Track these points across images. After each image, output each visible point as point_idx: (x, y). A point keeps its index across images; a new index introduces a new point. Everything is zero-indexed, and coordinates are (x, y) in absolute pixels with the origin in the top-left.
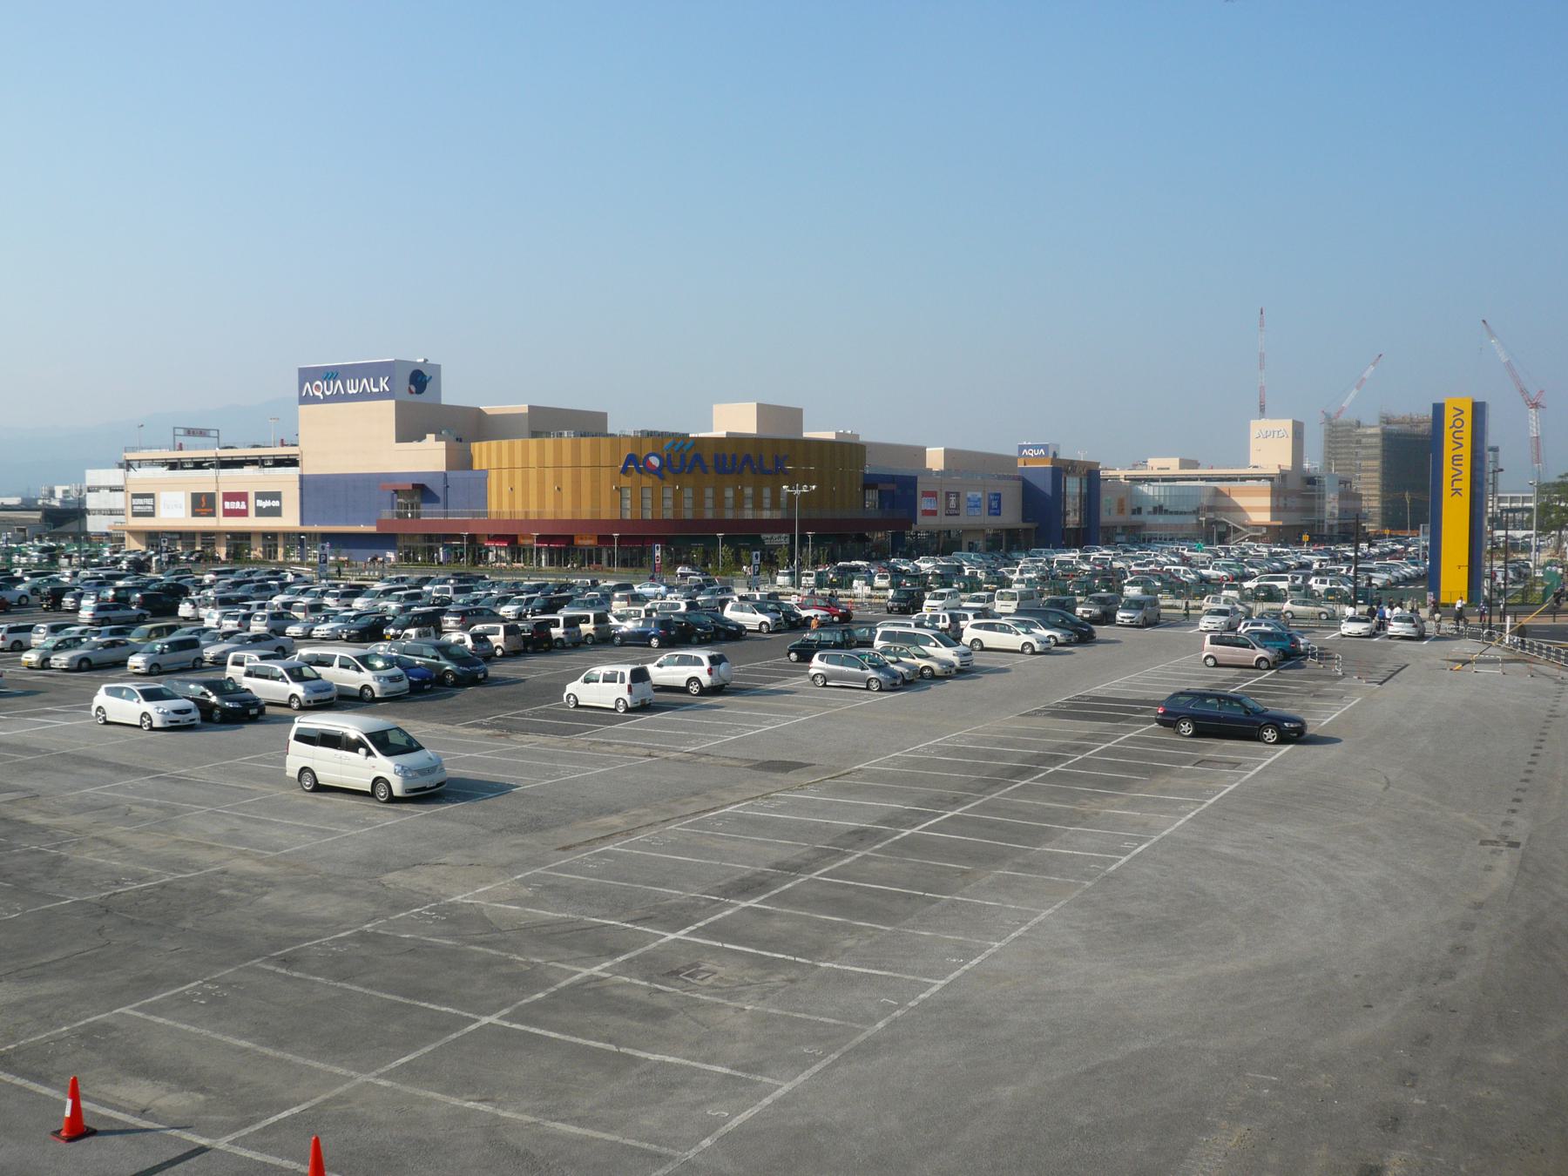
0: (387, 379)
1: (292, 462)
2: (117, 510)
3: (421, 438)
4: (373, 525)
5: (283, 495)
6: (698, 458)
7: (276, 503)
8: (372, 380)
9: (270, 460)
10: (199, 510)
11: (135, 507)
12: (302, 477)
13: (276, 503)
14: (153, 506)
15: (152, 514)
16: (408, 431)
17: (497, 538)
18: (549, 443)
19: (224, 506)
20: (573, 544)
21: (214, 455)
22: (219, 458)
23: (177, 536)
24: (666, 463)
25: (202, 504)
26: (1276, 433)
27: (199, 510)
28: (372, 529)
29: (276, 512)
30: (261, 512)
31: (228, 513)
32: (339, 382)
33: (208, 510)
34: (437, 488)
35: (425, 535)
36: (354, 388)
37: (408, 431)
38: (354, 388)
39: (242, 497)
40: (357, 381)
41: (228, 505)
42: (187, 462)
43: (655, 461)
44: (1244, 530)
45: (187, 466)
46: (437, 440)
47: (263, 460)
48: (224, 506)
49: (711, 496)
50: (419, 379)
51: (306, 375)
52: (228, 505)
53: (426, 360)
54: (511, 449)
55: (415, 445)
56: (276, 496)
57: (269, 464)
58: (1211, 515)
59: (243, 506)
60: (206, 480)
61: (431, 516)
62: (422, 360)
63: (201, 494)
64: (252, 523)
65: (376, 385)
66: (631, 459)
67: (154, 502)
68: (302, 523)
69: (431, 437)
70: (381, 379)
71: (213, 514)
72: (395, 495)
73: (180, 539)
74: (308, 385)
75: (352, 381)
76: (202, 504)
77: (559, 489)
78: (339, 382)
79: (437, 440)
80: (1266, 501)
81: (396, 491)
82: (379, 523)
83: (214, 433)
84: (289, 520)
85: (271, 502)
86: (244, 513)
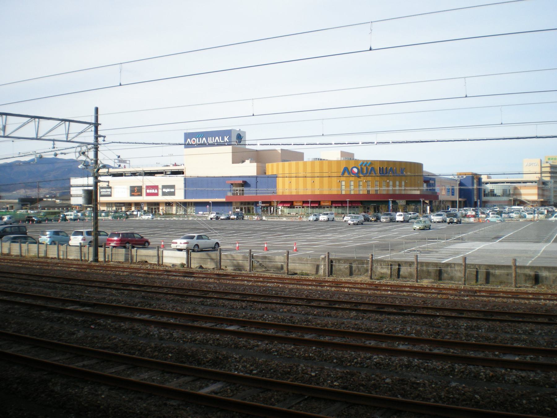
0: (228, 137)
1: (181, 173)
2: (75, 195)
3: (243, 162)
4: (224, 198)
5: (176, 187)
6: (373, 169)
7: (172, 190)
8: (221, 137)
9: (169, 172)
10: (133, 193)
11: (101, 193)
12: (185, 179)
13: (172, 190)
14: (111, 192)
15: (110, 196)
16: (238, 158)
17: (283, 203)
18: (287, 163)
19: (146, 191)
20: (293, 205)
21: (142, 170)
22: (144, 171)
23: (123, 205)
24: (361, 171)
25: (136, 191)
26: (534, 164)
27: (133, 193)
28: (224, 200)
29: (173, 194)
30: (164, 194)
31: (148, 194)
32: (204, 139)
33: (138, 193)
34: (252, 182)
35: (241, 202)
36: (212, 141)
37: (238, 158)
38: (212, 141)
39: (156, 187)
40: (213, 138)
41: (148, 191)
42: (128, 173)
43: (355, 170)
44: (528, 202)
45: (127, 175)
46: (251, 162)
47: (166, 172)
48: (146, 191)
49: (344, 185)
50: (240, 137)
51: (188, 136)
52: (148, 191)
53: (240, 130)
54: (290, 166)
55: (240, 165)
56: (173, 187)
57: (168, 173)
58: (515, 197)
59: (156, 191)
60: (137, 181)
61: (249, 194)
62: (239, 130)
63: (134, 187)
64: (160, 198)
65: (223, 139)
66: (346, 169)
67: (111, 190)
68: (185, 198)
69: (247, 162)
70: (225, 137)
71: (141, 195)
72: (232, 186)
73: (124, 206)
74: (189, 140)
75: (211, 138)
76: (136, 191)
77: (313, 182)
78: (204, 139)
79: (251, 162)
80: (535, 191)
81: (232, 184)
82: (227, 197)
83: (128, 162)
84: (179, 196)
85: (170, 190)
86: (156, 194)
